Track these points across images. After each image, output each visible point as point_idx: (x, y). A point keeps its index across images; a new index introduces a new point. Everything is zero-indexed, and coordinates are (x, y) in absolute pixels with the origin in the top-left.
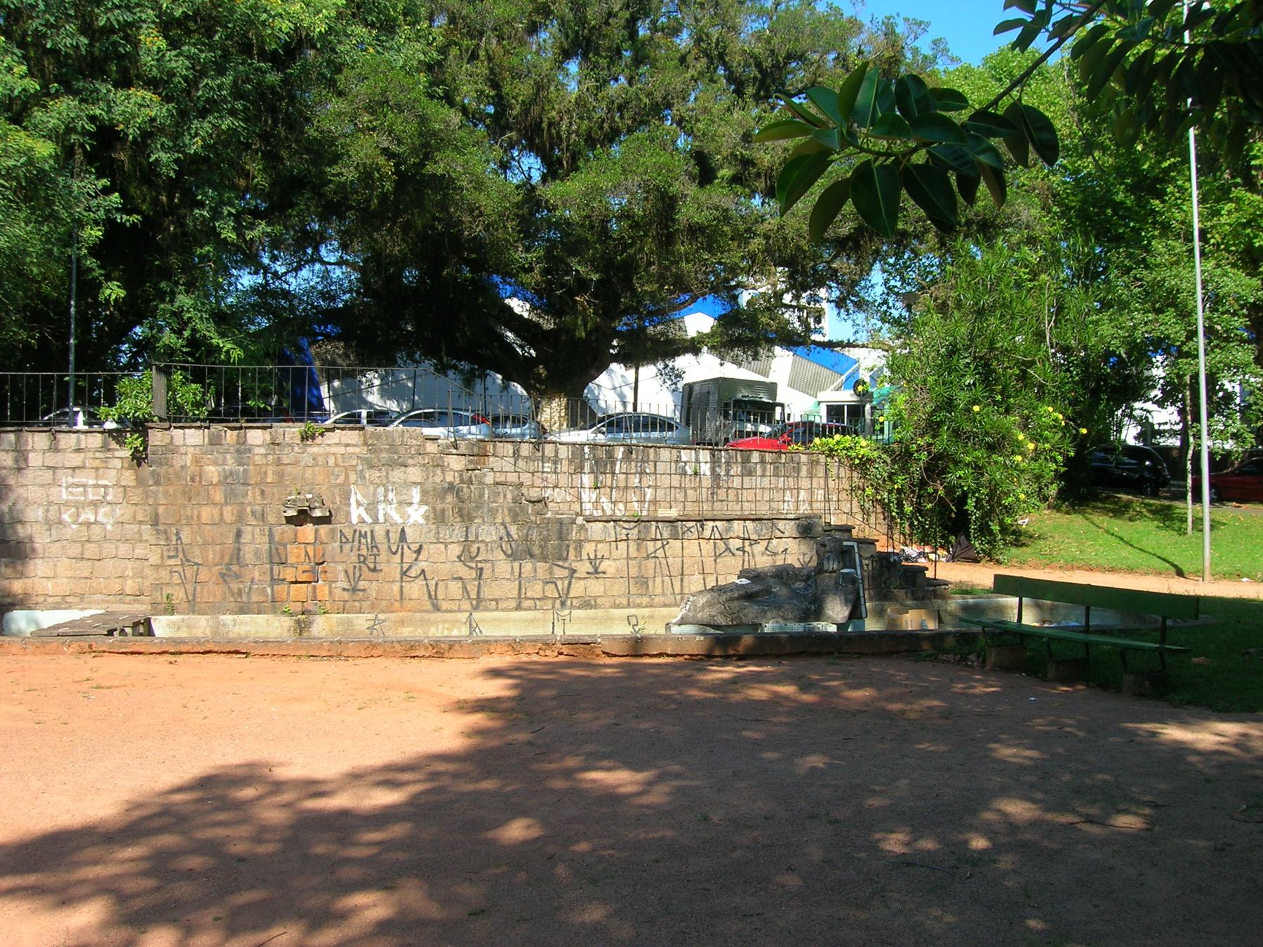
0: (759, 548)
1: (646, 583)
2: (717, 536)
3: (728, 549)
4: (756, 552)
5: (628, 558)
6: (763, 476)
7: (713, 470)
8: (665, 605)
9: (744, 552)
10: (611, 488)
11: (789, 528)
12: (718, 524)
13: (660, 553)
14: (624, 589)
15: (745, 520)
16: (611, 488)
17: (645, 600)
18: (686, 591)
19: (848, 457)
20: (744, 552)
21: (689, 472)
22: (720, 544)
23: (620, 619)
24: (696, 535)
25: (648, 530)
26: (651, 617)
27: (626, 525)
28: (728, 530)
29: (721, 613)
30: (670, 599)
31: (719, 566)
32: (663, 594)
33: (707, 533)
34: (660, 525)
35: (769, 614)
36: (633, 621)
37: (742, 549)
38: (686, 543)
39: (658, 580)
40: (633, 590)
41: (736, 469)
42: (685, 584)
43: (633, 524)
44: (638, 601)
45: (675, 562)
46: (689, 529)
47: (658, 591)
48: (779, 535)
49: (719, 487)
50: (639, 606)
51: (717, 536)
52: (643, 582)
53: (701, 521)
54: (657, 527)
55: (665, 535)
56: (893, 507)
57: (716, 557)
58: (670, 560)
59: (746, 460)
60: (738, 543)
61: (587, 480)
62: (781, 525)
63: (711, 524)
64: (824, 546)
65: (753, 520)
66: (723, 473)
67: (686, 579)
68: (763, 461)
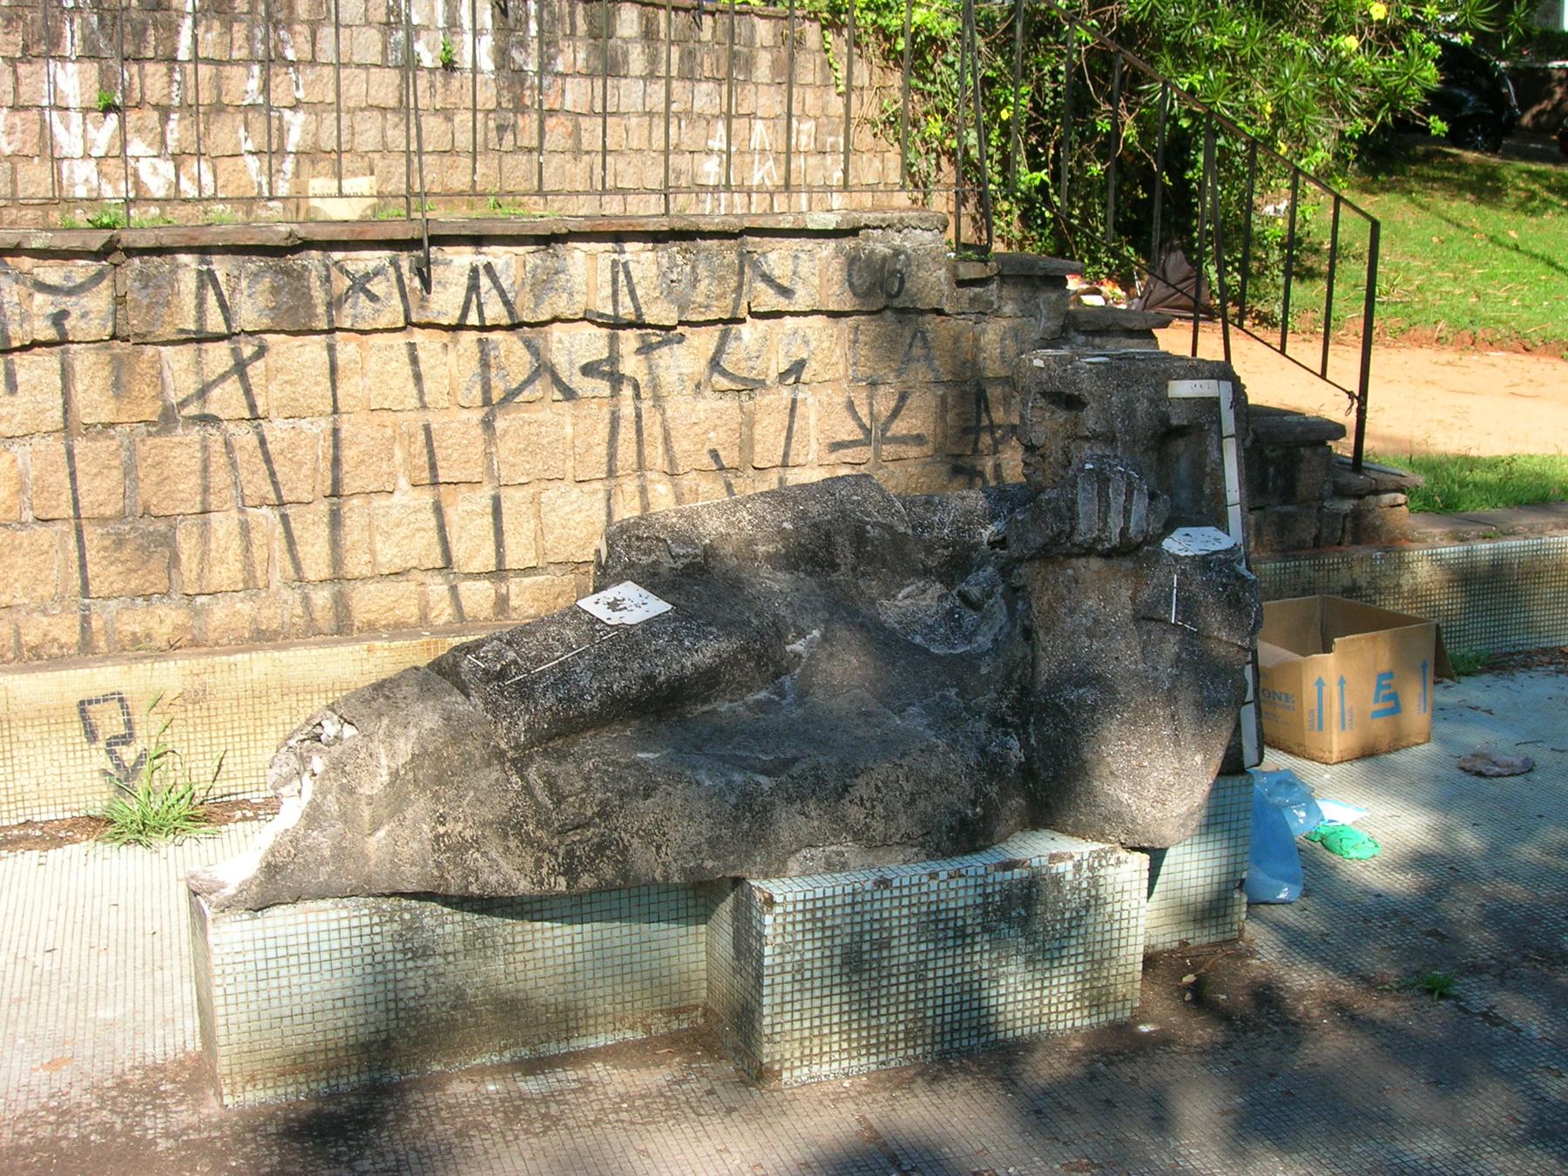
0: (684, 360)
1: (168, 541)
2: (495, 311)
3: (543, 369)
4: (668, 378)
5: (69, 427)
6: (651, 76)
7: (502, 56)
8: (262, 638)
9: (616, 379)
10: (164, 111)
11: (814, 272)
12: (498, 256)
13: (227, 400)
14: (59, 570)
15: (619, 237)
16: (164, 111)
17: (166, 619)
18: (356, 564)
19: (881, 30)
20: (616, 379)
21: (428, 60)
22: (511, 352)
23: (44, 717)
24: (393, 313)
25: (160, 292)
26: (196, 698)
27: (52, 273)
28: (542, 285)
29: (507, 827)
30: (282, 607)
31: (504, 449)
32: (250, 585)
33: (446, 301)
34: (221, 266)
35: (788, 823)
36: (109, 722)
37: (607, 371)
38: (348, 348)
39: (224, 524)
40: (104, 577)
41: (573, 56)
42: (353, 531)
43: (82, 270)
44: (132, 622)
45: (299, 441)
46: (361, 284)
47: (226, 571)
48: (768, 299)
49: (520, 108)
50: (137, 648)
51: (495, 311)
52: (150, 538)
53: (419, 246)
54: (207, 279)
55: (249, 313)
56: (992, 171)
57: (492, 406)
58: (277, 430)
59: (601, 32)
60: (588, 343)
61: (73, 81)
62: (778, 257)
63: (462, 258)
64: (1071, 402)
65: (657, 238)
66: (532, 66)
67: (354, 512)
68: (649, 34)
